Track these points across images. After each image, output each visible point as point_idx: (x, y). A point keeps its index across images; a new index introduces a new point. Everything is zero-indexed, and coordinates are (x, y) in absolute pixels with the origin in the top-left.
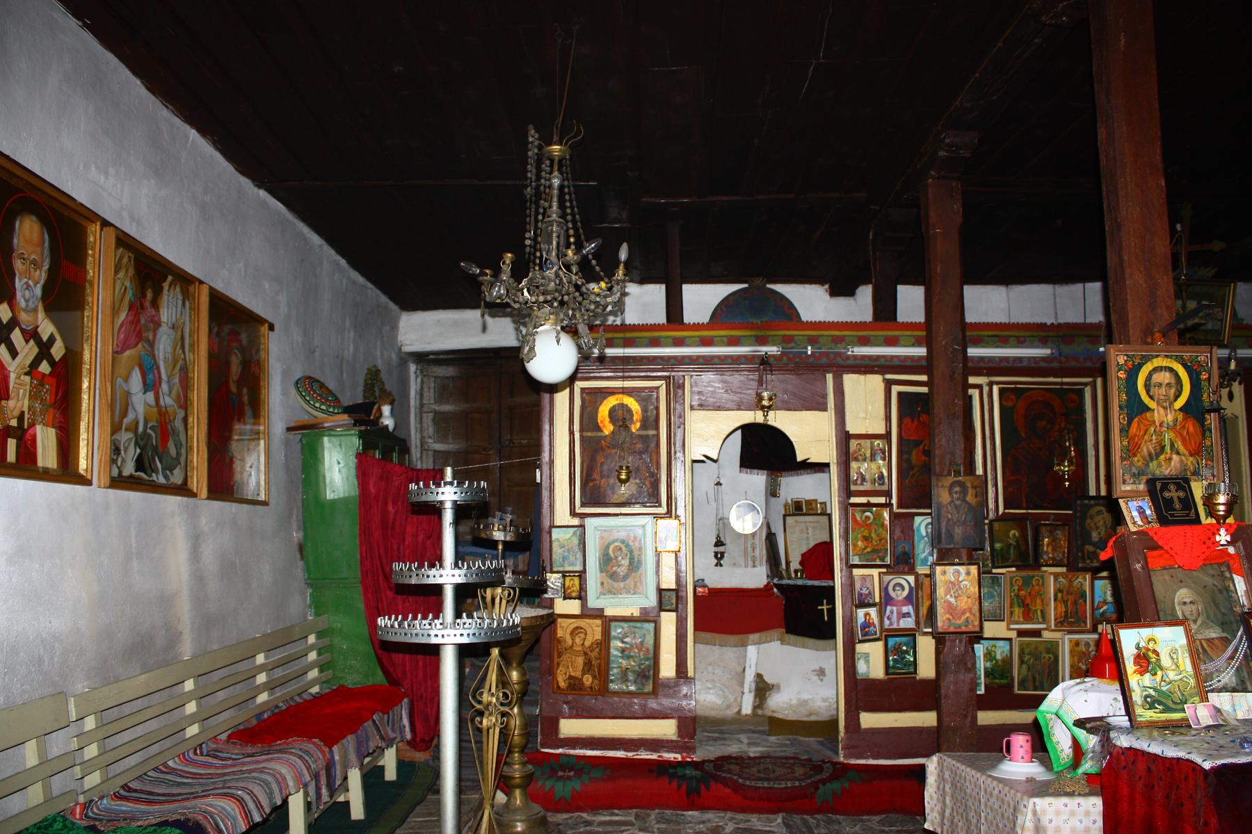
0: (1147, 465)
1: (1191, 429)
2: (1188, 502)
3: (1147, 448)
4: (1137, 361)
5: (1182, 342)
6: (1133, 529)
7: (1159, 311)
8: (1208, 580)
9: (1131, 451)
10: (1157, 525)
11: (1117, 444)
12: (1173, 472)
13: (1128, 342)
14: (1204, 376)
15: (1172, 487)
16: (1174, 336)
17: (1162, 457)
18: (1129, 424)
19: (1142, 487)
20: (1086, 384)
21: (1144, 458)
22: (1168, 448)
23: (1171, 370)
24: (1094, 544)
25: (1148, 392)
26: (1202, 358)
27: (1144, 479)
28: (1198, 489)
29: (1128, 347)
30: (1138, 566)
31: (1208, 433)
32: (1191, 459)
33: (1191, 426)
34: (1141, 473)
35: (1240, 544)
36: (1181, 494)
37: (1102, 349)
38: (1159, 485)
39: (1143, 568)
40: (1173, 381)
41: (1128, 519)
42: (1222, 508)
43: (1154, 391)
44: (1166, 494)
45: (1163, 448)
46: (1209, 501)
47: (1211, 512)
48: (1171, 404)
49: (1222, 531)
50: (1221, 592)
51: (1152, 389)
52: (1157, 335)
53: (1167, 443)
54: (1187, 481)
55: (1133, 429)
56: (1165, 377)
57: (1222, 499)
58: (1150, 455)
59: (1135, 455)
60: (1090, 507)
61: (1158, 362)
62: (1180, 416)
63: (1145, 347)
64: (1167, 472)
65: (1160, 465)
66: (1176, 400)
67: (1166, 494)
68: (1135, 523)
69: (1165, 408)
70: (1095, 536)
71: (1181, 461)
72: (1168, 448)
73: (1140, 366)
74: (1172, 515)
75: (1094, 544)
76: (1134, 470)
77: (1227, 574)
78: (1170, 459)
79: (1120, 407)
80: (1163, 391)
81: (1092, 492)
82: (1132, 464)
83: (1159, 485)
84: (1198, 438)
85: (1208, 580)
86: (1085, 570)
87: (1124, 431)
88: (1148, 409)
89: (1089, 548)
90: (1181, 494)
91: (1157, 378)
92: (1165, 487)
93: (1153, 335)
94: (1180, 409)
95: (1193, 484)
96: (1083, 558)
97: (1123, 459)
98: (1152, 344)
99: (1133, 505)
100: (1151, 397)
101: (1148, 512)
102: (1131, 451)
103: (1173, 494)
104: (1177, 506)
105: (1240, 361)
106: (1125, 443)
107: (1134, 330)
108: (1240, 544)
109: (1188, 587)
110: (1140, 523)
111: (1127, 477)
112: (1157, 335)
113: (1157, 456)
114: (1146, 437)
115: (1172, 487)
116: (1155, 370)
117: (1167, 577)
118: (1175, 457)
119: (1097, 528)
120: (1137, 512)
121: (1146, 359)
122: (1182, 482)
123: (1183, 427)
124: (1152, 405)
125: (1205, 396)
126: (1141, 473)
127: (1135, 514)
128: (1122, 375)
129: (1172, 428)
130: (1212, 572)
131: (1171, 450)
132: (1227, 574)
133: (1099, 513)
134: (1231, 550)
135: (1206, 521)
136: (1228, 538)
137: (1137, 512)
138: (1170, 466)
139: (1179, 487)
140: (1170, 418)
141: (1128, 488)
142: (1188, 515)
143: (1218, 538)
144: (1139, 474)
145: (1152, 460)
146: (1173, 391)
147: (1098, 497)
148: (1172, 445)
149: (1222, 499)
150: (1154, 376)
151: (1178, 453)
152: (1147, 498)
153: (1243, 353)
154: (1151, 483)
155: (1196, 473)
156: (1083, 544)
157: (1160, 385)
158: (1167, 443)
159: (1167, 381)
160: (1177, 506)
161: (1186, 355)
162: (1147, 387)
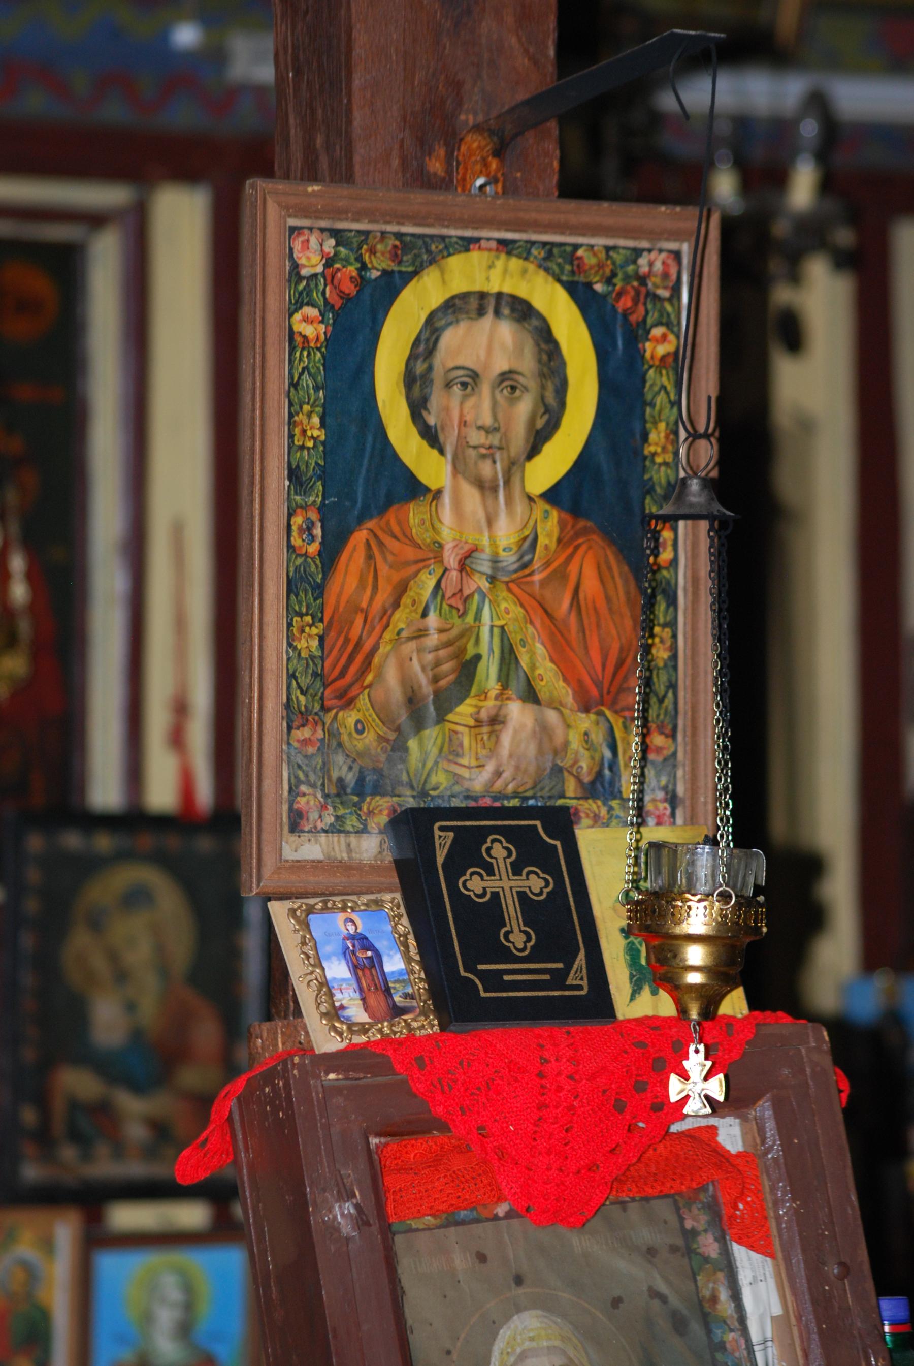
0: (399, 747)
1: (591, 585)
2: (564, 921)
3: (401, 666)
4: (378, 264)
5: (578, 186)
6: (326, 1041)
7: (487, 27)
8: (631, 1273)
9: (333, 680)
10: (425, 1026)
11: (275, 642)
12: (508, 783)
13: (343, 173)
14: (659, 346)
15: (499, 852)
16: (545, 151)
17: (465, 710)
18: (330, 555)
19: (371, 847)
20: (96, 220)
21: (386, 718)
22: (489, 672)
23: (522, 311)
24: (107, 1067)
25: (417, 409)
26: (653, 263)
27: (381, 809)
28: (607, 862)
29: (341, 194)
30: (342, 1213)
31: (661, 606)
32: (585, 722)
33: (595, 572)
34: (368, 785)
35: (764, 1109)
36: (536, 883)
37: (186, 36)
38: (443, 842)
39: (361, 1220)
40: (527, 364)
41: (306, 995)
42: (696, 955)
43: (444, 405)
44: (475, 884)
45: (468, 669)
46: (651, 916)
47: (660, 967)
48: (513, 469)
49: (696, 1061)
50: (679, 1324)
51: (436, 400)
52: (474, 143)
53: (487, 647)
54: (562, 822)
55: (347, 579)
56: (492, 345)
57: (698, 918)
58: (412, 700)
59: (347, 701)
60: (89, 866)
61: (466, 272)
62: (549, 525)
63: (419, 199)
64: (478, 782)
65: (451, 750)
66: (533, 451)
67: (475, 884)
68: (334, 1013)
69: (486, 488)
70: (108, 1022)
71: (543, 730)
72: (489, 672)
73: (390, 287)
74: (494, 981)
75: (107, 1067)
76: (341, 769)
77: (709, 1245)
78: (496, 721)
79: (294, 474)
80: (483, 406)
81: (105, 791)
82: (333, 740)
83: (443, 842)
84: (620, 629)
85: (631, 1273)
86: (49, 1197)
87: (307, 587)
88: (414, 488)
89: (77, 1083)
90: (536, 883)
91: (463, 344)
92: (468, 852)
93: (452, 140)
94: (552, 496)
95: (587, 838)
96: (44, 1138)
97: (294, 716)
98: (445, 184)
99: (333, 927)
100: (431, 436)
101: (393, 964)
102: (333, 680)
103: (502, 881)
104: (517, 936)
105: (835, 137)
106: (309, 644)
107: (375, 114)
108: (764, 1109)
109: (546, 1304)
110: (357, 1013)
111: (309, 800)
112: (474, 143)
113: (445, 704)
114: (400, 619)
115: (499, 852)
116: (456, 307)
117: (461, 1262)
118: (516, 711)
119: (122, 976)
120: (342, 966)
121: (416, 256)
122: (543, 833)
123: (560, 575)
124: (431, 468)
125: (657, 436)
126: (368, 785)
127: (338, 970)
128: (310, 325)
129: (516, 577)
130: (645, 1235)
131: (504, 679)
132: (709, 1245)
133: (137, 898)
134: (731, 1135)
135: (636, 1003)
136: (716, 1088)
137: (342, 966)
138: (484, 757)
139: (530, 853)
140: (507, 533)
141: (311, 849)
142: (559, 979)
143: (675, 1088)
144: (360, 789)
145: (418, 723)
146: (524, 407)
147: (134, 819)
148: (508, 657)
149: (698, 918)
150: (450, 338)
151: (531, 696)
152: (393, 898)
153: (866, 97)
154: (414, 826)
155: (601, 786)
156: (47, 1064)
157: (471, 380)
158: (487, 647)
159: (501, 364)
160: (517, 936)
161: (591, 246)
162: (416, 385)
